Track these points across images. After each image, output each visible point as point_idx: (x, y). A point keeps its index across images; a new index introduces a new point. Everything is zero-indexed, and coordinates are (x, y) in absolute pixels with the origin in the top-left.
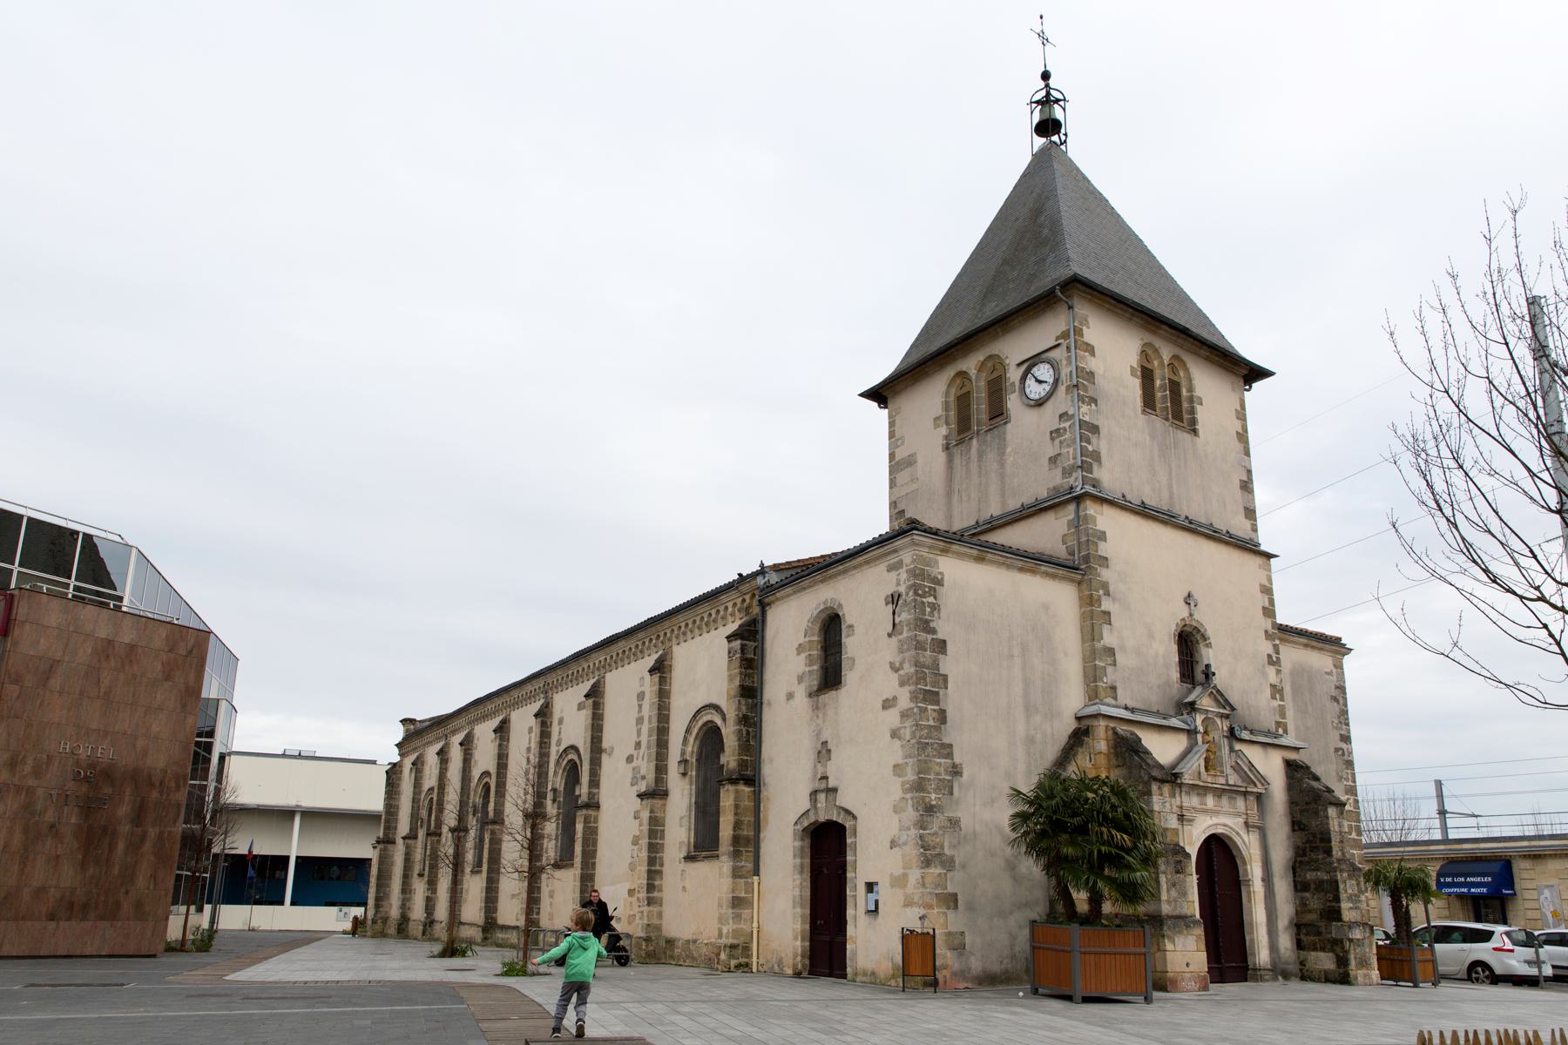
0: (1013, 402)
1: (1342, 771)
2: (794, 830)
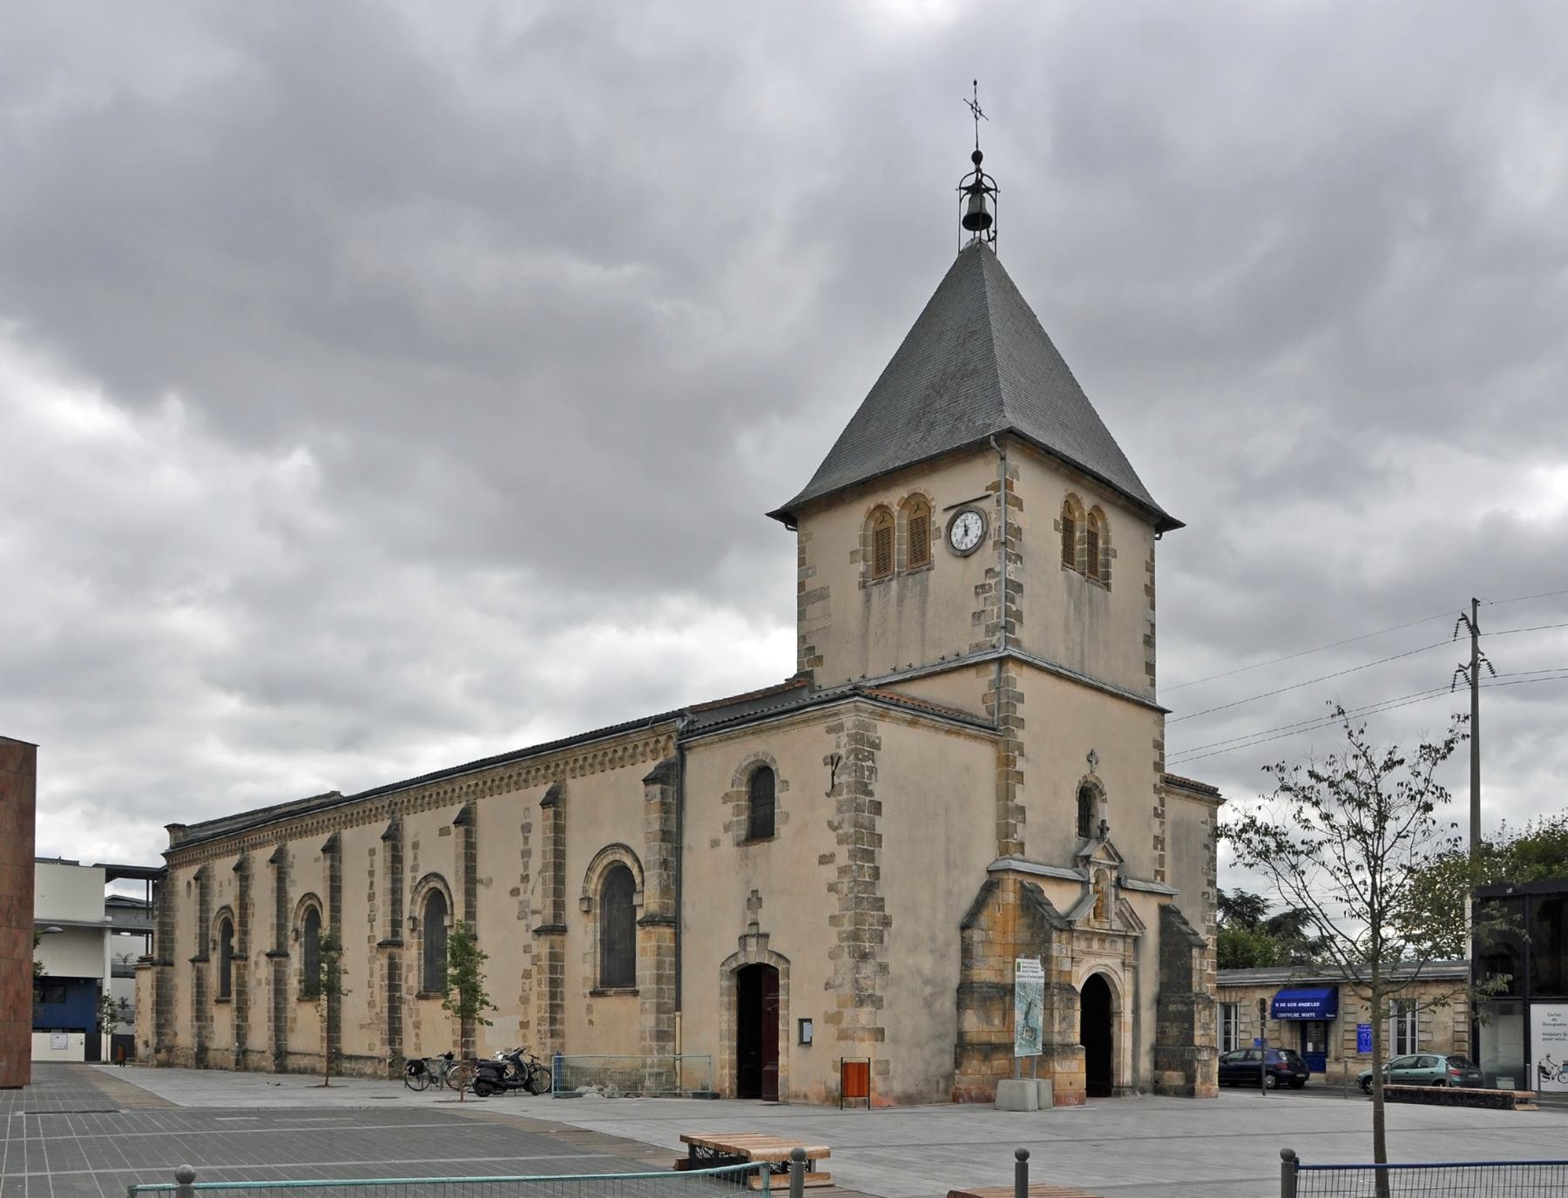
0: (937, 548)
1: (1206, 913)
2: (721, 970)
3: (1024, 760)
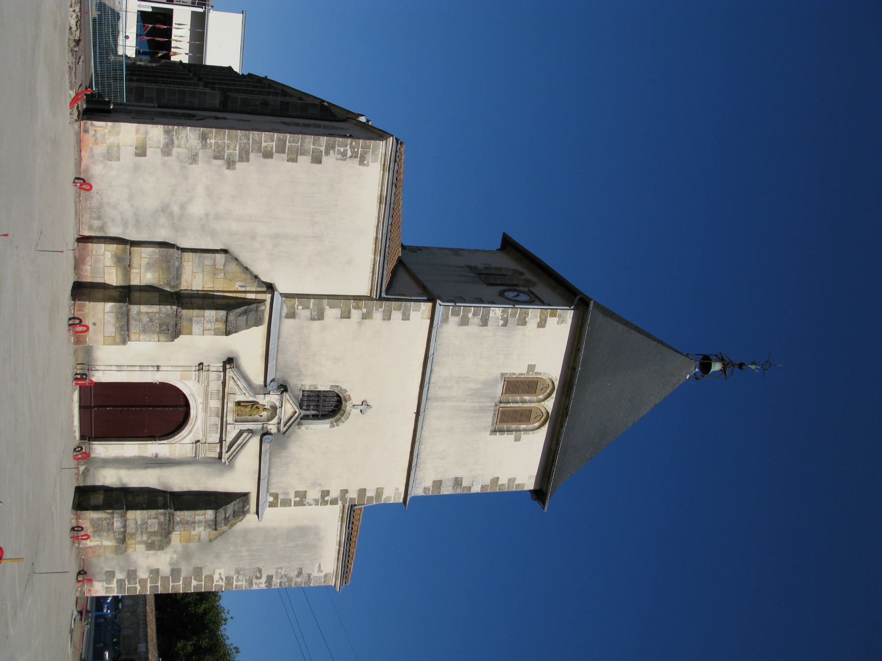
3: (360, 320)
